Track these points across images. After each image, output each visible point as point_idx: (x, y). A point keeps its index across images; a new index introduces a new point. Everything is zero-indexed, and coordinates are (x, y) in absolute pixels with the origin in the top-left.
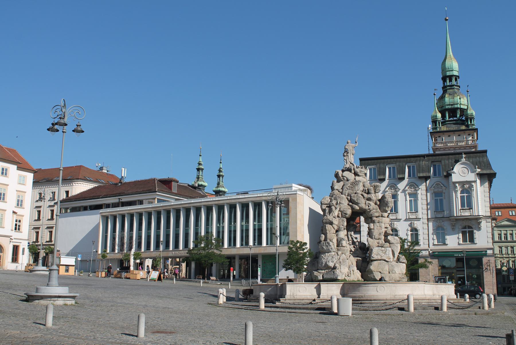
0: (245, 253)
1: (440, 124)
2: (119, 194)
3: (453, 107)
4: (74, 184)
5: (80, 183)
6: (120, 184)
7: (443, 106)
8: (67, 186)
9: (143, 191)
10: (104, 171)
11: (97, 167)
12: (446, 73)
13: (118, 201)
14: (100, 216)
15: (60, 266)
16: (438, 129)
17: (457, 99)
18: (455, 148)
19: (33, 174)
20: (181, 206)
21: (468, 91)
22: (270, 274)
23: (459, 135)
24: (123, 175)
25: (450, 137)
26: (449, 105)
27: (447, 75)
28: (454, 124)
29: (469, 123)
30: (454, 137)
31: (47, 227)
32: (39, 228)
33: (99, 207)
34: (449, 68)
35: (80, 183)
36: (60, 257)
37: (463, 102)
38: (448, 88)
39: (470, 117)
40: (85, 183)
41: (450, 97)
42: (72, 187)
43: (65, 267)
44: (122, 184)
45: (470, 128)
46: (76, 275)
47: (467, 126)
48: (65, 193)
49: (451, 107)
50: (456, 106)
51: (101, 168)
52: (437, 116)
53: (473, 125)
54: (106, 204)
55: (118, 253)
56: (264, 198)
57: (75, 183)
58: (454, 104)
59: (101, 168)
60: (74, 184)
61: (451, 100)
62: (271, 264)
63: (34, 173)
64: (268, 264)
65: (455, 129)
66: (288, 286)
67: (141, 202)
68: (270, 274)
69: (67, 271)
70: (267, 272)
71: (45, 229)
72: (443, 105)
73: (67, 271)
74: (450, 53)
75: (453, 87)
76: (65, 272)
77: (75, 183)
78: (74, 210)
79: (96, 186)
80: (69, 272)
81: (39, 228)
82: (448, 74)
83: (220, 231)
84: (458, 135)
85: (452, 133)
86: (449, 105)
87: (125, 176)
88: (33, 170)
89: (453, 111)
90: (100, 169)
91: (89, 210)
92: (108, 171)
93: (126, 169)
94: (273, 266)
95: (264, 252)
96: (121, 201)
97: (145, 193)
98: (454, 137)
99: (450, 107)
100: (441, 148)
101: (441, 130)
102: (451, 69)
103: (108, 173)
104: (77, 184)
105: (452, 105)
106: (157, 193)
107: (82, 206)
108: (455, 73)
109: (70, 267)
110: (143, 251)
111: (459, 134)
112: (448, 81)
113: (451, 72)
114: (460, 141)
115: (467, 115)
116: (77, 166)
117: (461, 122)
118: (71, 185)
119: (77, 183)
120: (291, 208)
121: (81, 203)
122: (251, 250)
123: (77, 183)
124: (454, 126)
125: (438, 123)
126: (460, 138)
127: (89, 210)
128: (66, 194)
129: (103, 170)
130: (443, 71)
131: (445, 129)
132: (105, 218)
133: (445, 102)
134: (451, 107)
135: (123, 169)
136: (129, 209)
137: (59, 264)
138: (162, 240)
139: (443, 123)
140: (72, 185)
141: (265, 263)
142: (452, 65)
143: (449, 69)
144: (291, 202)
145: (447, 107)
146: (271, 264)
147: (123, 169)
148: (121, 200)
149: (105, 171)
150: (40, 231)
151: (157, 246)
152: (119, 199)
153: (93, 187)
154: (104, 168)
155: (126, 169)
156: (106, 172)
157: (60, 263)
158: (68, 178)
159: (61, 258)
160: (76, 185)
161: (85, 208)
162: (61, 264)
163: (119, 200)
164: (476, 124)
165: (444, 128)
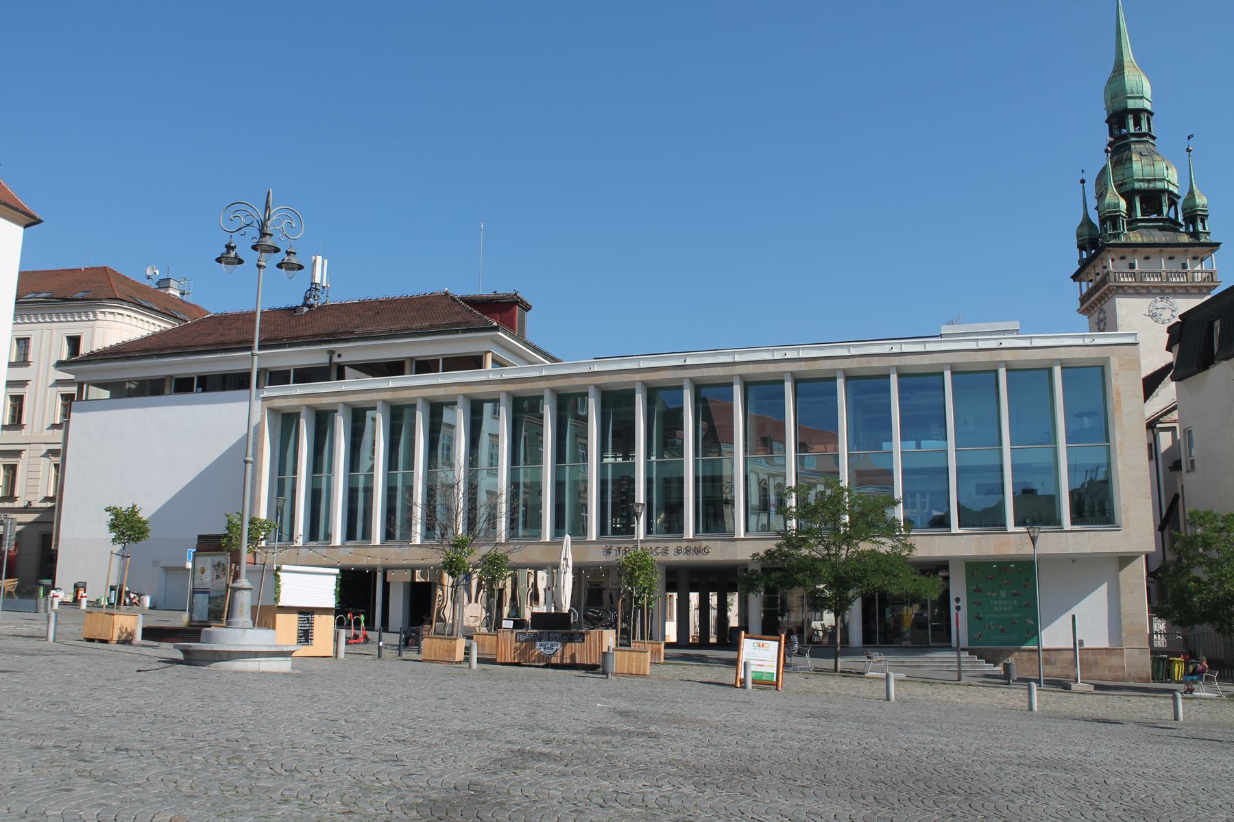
0: (937, 555)
1: (1125, 227)
2: (329, 335)
3: (1151, 186)
4: (100, 316)
5: (122, 314)
6: (306, 309)
7: (1126, 183)
8: (75, 321)
9: (431, 326)
10: (171, 291)
11: (148, 277)
12: (1126, 102)
13: (327, 361)
14: (262, 411)
15: (278, 616)
16: (1123, 240)
17: (1160, 166)
18: (1164, 290)
19: (21, 230)
20: (637, 377)
21: (1188, 150)
22: (1003, 631)
23: (1147, 258)
24: (317, 280)
25: (1150, 260)
26: (1142, 180)
27: (1129, 107)
28: (1161, 229)
29: (1200, 228)
30: (1163, 260)
31: (48, 450)
32: (18, 453)
33: (238, 381)
34: (1134, 90)
35: (122, 314)
36: (279, 569)
37: (1172, 177)
38: (1132, 139)
39: (1200, 213)
40: (136, 315)
41: (1145, 161)
42: (93, 325)
43: (295, 617)
44: (312, 309)
45: (1202, 240)
46: (342, 654)
47: (1195, 234)
48: (66, 342)
49: (1146, 185)
50: (1159, 185)
51: (164, 283)
52: (1121, 204)
53: (1208, 234)
54: (271, 372)
55: (343, 546)
56: (1007, 356)
57: (104, 312)
58: (1155, 180)
59: (164, 283)
60: (100, 316)
61: (1148, 169)
62: (1003, 594)
63: (26, 226)
64: (994, 595)
65: (1163, 240)
66: (505, 622)
67: (475, 362)
68: (1003, 631)
69: (305, 636)
70: (992, 623)
71: (42, 456)
72: (1125, 181)
73: (305, 636)
74: (1128, 56)
75: (1144, 139)
76: (299, 642)
77: (104, 312)
78: (153, 388)
79: (169, 327)
80: (314, 642)
81: (18, 453)
82: (1131, 104)
83: (652, 478)
84: (1143, 257)
85: (1157, 249)
86: (1142, 180)
87: (324, 285)
88: (23, 209)
89: (1152, 198)
90: (158, 283)
91: (200, 389)
92: (183, 294)
93: (326, 261)
94: (1015, 602)
95: (1021, 552)
96: (336, 359)
97: (446, 334)
98: (1163, 260)
99: (1144, 186)
100: (1129, 287)
101: (1129, 241)
102: (1138, 93)
103: (185, 298)
104: (110, 317)
105: (1149, 181)
106: (500, 334)
107: (171, 377)
108: (1148, 106)
109: (316, 617)
110: (548, 540)
111: (1171, 255)
112: (1131, 122)
113: (1138, 101)
114: (1177, 272)
115: (1191, 208)
116: (92, 269)
117: (1172, 225)
118: (87, 316)
119: (110, 313)
120: (1118, 394)
121: (167, 365)
122: (1037, 545)
123: (110, 313)
124: (1159, 233)
125: (1121, 221)
126: (1176, 266)
127: (197, 392)
128: (69, 344)
129: (169, 287)
130: (1116, 97)
131: (1139, 240)
132: (286, 422)
133: (1133, 173)
134: (1146, 185)
135: (319, 259)
136: (391, 385)
137: (271, 603)
138: (642, 502)
139: (1132, 224)
140: (91, 317)
141: (978, 590)
142: (1140, 83)
143: (1132, 93)
144: (1117, 374)
145: (1137, 185)
146: (1003, 594)
147: (319, 259)
148: (339, 356)
149: (174, 292)
150: (22, 465)
151: (355, 528)
152: (331, 353)
153: (157, 330)
154: (172, 283)
155: (326, 261)
156: (177, 294)
157: (277, 600)
158: (79, 295)
159: (282, 575)
160: (107, 318)
161: (183, 385)
162: (280, 604)
163: (331, 359)
164: (1213, 229)
165: (1135, 237)
